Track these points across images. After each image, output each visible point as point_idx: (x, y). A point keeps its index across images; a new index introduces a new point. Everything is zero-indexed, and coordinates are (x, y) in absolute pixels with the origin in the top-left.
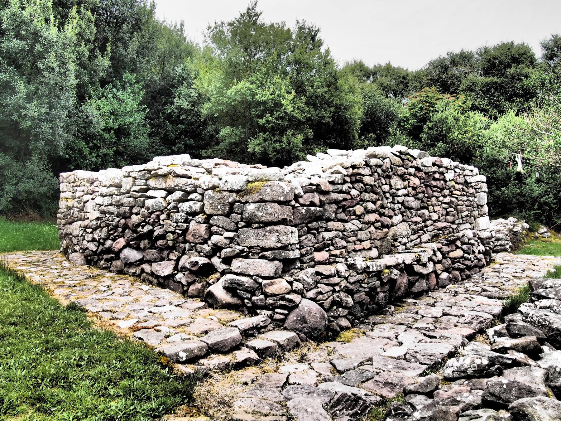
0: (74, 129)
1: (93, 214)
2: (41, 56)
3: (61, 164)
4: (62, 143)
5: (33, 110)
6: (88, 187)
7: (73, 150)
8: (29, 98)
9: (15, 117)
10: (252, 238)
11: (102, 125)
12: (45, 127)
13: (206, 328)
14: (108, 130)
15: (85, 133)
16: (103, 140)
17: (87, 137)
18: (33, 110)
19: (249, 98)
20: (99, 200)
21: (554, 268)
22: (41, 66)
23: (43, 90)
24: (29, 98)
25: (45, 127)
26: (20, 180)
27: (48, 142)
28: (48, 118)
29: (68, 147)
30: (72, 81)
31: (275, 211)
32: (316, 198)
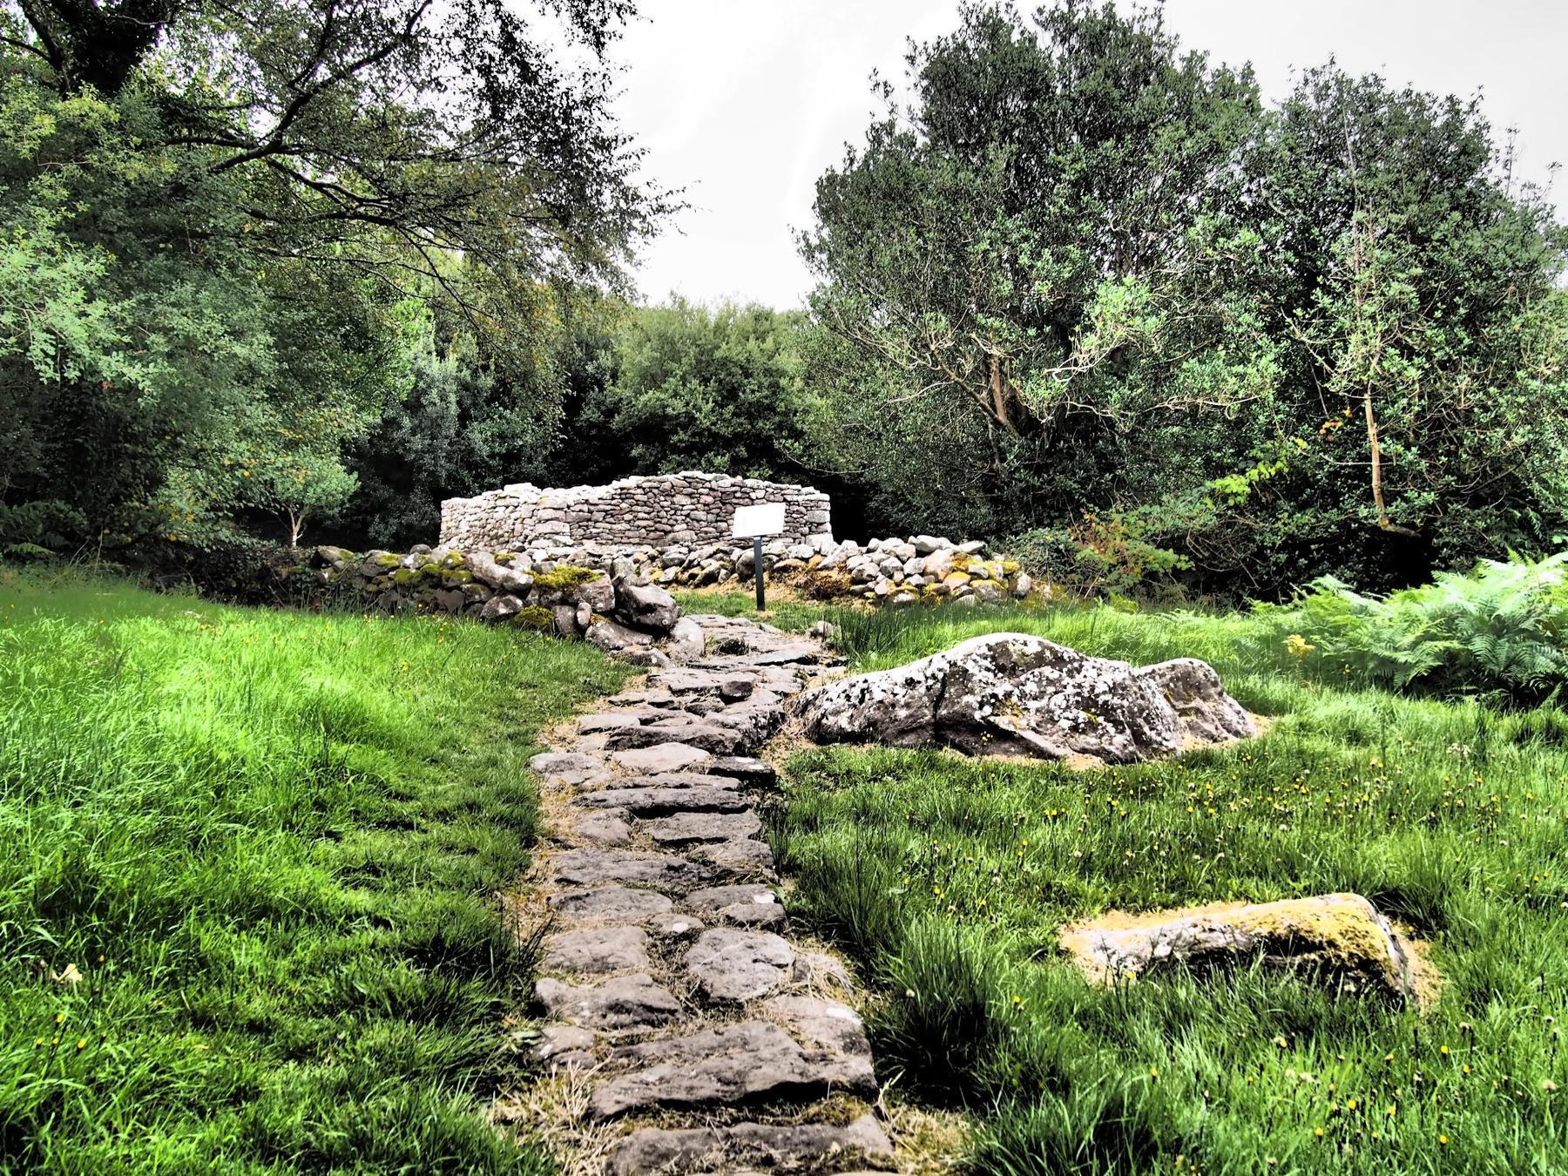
0: (457, 457)
1: (464, 527)
2: (425, 392)
3: (439, 494)
4: (444, 474)
5: (418, 443)
6: (462, 510)
7: (456, 480)
8: (413, 432)
9: (400, 451)
10: (542, 528)
11: (486, 451)
12: (428, 458)
13: (721, 834)
14: (492, 456)
15: (468, 459)
16: (489, 467)
17: (470, 466)
18: (418, 443)
19: (660, 412)
20: (469, 518)
21: (350, 474)
22: (425, 402)
23: (426, 423)
24: (413, 432)
25: (428, 458)
26: (403, 512)
27: (432, 474)
28: (431, 449)
29: (449, 476)
30: (454, 409)
31: (550, 514)
32: (585, 508)
